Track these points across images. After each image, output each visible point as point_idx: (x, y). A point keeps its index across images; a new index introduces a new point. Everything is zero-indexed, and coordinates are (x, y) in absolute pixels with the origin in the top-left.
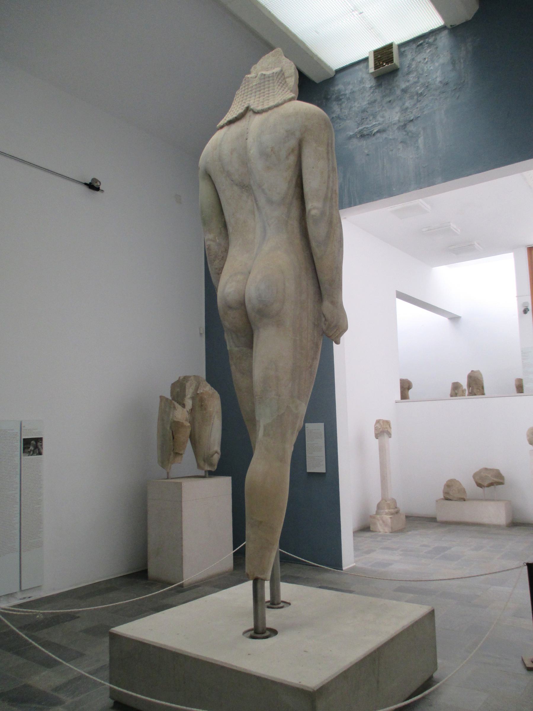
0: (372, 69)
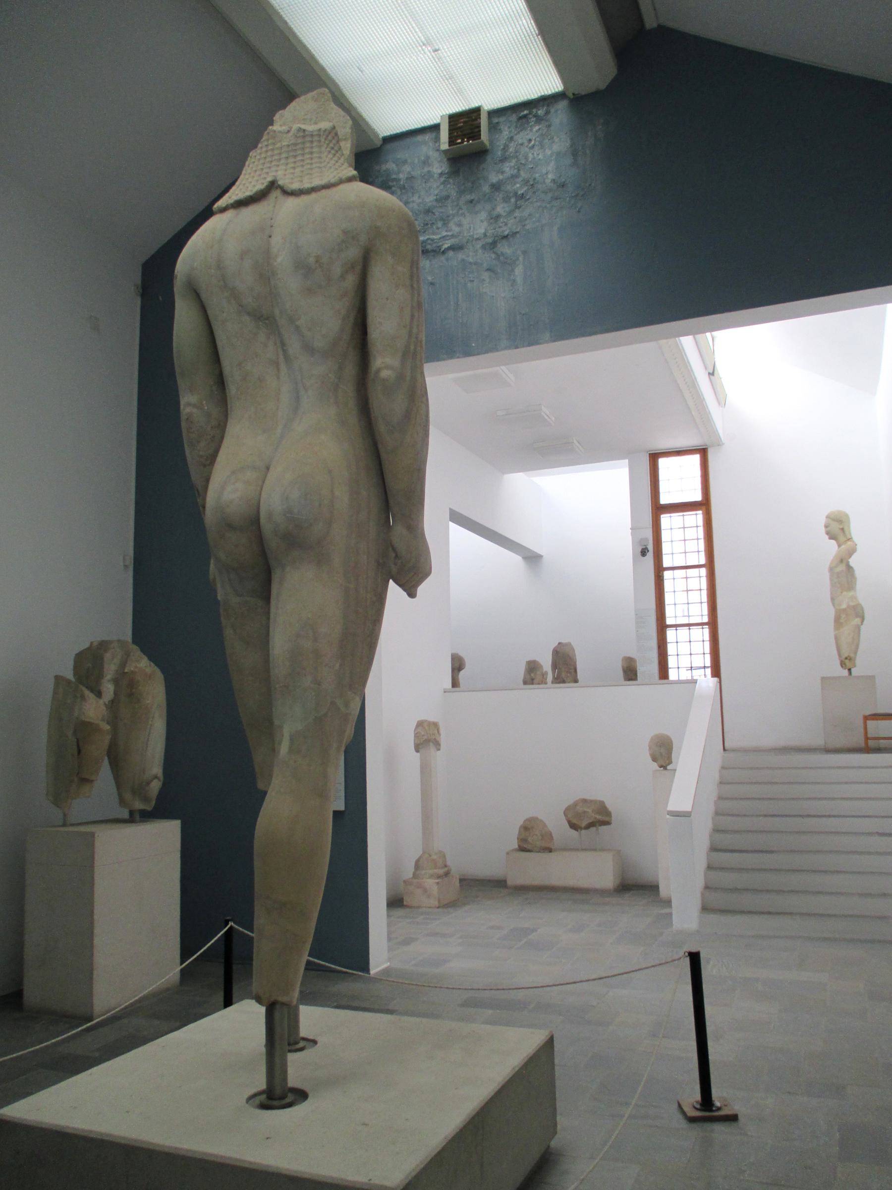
0: (444, 145)
